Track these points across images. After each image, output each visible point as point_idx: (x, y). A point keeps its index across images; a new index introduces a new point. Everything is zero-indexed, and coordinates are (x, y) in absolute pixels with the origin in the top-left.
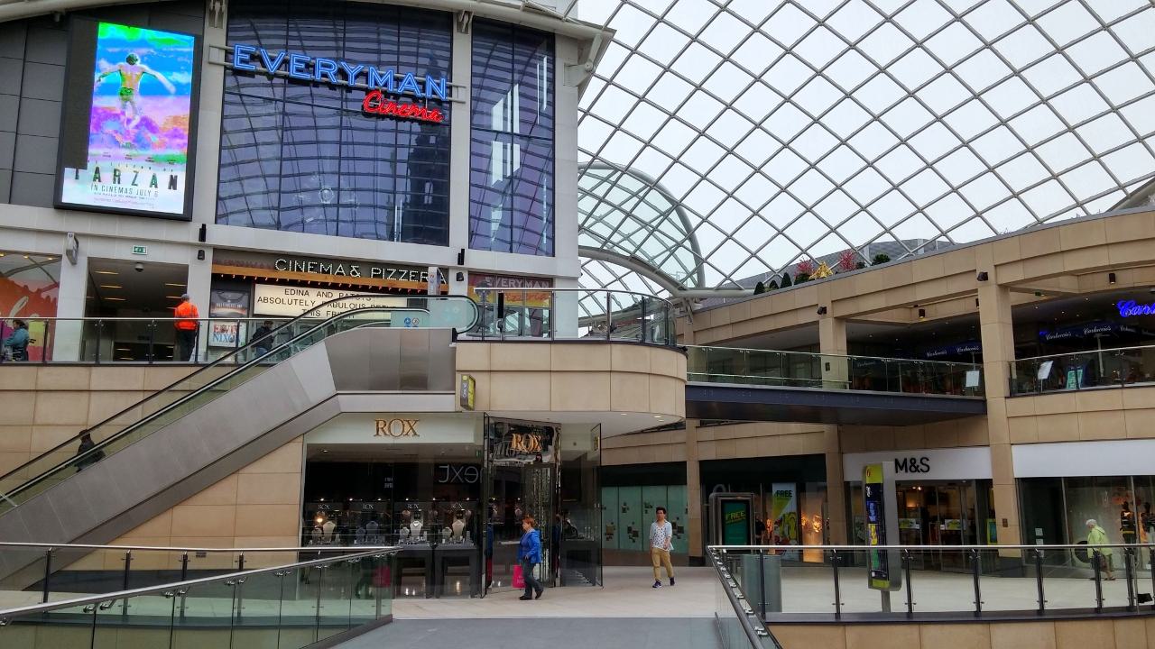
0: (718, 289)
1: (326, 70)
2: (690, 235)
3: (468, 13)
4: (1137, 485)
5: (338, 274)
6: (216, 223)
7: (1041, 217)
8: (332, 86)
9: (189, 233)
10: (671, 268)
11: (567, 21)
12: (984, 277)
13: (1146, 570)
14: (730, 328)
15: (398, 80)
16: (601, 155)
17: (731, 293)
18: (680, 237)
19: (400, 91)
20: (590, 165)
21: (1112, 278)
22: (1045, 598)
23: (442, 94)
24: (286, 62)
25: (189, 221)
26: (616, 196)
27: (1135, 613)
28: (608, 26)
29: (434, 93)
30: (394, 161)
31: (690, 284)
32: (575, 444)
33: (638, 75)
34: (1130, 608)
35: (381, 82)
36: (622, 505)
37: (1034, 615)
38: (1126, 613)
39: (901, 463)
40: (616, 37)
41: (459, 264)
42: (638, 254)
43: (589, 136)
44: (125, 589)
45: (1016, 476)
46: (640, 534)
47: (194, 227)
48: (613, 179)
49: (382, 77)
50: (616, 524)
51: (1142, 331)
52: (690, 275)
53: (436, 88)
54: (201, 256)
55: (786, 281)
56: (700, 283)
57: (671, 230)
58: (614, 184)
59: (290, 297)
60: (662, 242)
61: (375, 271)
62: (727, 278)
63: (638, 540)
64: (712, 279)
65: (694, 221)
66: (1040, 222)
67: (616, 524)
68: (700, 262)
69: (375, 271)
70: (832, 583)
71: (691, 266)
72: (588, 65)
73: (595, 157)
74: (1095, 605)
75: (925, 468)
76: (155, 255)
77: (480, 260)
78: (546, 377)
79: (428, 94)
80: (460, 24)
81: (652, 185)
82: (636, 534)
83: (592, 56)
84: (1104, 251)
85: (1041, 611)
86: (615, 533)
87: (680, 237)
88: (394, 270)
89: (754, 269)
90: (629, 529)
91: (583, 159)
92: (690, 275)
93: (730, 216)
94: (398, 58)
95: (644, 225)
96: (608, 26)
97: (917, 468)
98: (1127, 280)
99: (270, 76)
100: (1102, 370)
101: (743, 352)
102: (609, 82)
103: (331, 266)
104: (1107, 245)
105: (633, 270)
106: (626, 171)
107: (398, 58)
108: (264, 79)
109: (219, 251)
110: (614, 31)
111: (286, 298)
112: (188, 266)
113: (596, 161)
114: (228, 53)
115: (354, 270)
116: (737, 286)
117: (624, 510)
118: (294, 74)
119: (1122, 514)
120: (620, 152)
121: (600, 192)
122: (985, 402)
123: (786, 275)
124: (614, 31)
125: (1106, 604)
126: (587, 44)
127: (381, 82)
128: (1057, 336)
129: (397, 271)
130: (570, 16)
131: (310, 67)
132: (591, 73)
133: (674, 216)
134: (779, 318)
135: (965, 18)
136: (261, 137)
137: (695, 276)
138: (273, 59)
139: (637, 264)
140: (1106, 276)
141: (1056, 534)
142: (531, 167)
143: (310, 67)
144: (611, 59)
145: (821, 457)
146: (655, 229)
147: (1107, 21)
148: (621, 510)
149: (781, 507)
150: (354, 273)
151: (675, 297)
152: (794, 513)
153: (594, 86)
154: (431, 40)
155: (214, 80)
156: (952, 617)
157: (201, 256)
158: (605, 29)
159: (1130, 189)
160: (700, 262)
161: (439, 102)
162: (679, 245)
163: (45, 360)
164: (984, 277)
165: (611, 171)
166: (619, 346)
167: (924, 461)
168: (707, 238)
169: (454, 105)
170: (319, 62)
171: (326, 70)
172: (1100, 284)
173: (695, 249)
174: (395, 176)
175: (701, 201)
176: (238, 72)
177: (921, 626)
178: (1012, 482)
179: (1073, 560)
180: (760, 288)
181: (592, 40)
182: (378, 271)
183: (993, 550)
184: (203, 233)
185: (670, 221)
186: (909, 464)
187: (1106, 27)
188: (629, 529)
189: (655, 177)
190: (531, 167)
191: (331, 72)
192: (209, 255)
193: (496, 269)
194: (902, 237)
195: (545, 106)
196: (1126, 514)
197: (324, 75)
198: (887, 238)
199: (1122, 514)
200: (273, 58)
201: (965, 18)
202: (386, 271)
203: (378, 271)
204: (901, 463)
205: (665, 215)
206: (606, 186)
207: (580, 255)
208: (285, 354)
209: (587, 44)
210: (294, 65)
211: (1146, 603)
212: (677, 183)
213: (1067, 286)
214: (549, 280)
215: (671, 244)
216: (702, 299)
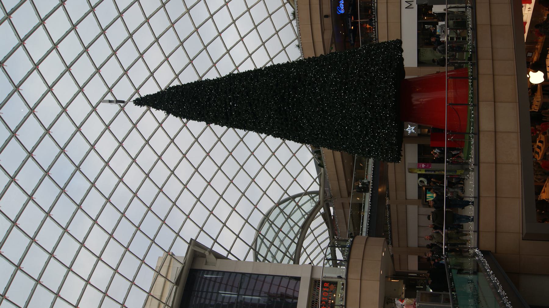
0: (320, 185)
2: (293, 198)
7: (295, 37)
10: (308, 207)
11: (185, 263)
17: (323, 179)
18: (293, 204)
21: (326, 16)
26: (270, 235)
31: (317, 199)
33: (213, 227)
40: (194, 238)
42: (300, 224)
43: (240, 251)
45: (416, 66)
51: (351, 3)
52: (312, 198)
56: (317, 193)
57: (290, 207)
58: (264, 237)
62: (315, 180)
64: (316, 187)
65: (286, 196)
66: (297, 38)
71: (307, 198)
72: (207, 253)
73: (251, 247)
81: (266, 217)
83: (202, 251)
84: (315, 26)
89: (312, 168)
91: (251, 258)
92: (312, 198)
93: (285, 179)
95: (287, 249)
98: (327, 10)
102: (215, 241)
104: (311, 24)
106: (259, 231)
110: (192, 239)
113: (254, 247)
116: (319, 177)
120: (249, 235)
121: (268, 244)
124: (192, 239)
126: (197, 252)
130: (182, 261)
132: (211, 251)
133: (282, 206)
137: (313, 195)
139: (305, 227)
142: (255, 285)
144: (206, 242)
153: (217, 249)
158: (190, 244)
160: (306, 193)
166: (349, 275)
168: (295, 190)
172: (328, 22)
173: (300, 195)
175: (276, 194)
181: (195, 251)
187: (135, 126)
189: (262, 216)
190: (255, 285)
195: (223, 295)
205: (282, 211)
207: (298, 264)
209: (197, 252)
212: (266, 206)
213: (329, 35)
216: (325, 192)
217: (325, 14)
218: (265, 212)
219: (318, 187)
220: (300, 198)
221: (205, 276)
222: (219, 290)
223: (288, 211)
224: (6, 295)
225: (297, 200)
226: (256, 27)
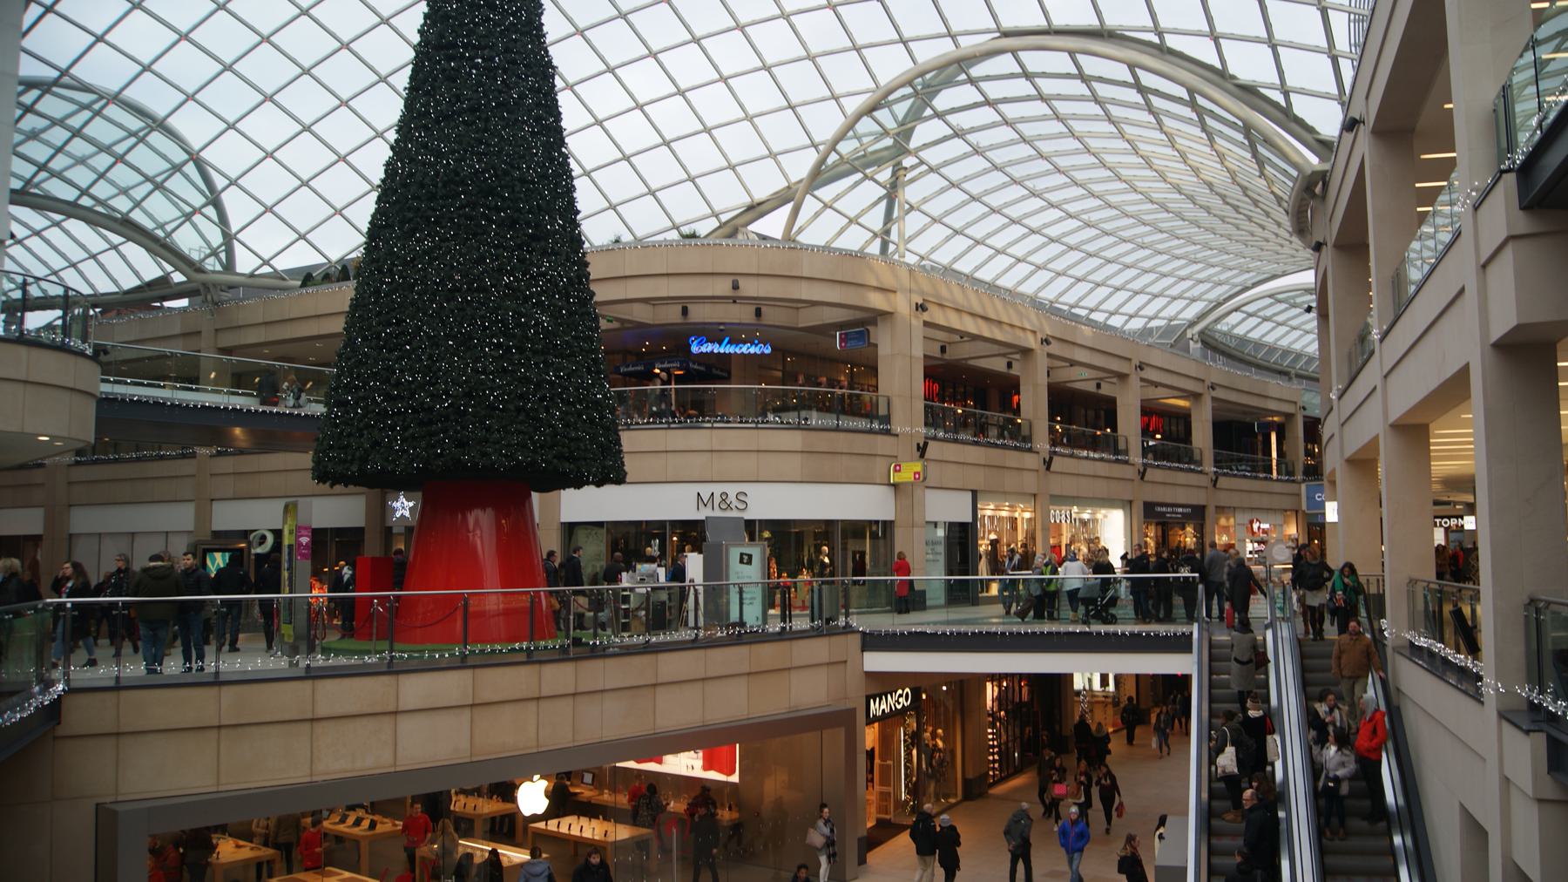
0: (252, 275)
4: (845, 537)
7: (639, 234)
14: (263, 329)
16: (72, 71)
17: (269, 285)
18: (198, 200)
20: (56, 82)
31: (212, 264)
44: (1187, 814)
45: (563, 520)
48: (97, 107)
55: (327, 278)
56: (229, 266)
58: (98, 113)
64: (245, 263)
65: (220, 182)
68: (228, 238)
71: (216, 238)
73: (64, 73)
75: (741, 506)
87: (198, 200)
89: (301, 257)
93: (269, 182)
105: (129, 239)
106: (116, 99)
113: (63, 81)
120: (103, 70)
121: (76, 122)
123: (345, 268)
133: (190, 169)
134: (632, 283)
140: (679, 308)
147: (307, 122)
151: (189, 280)
159: (724, 218)
160: (228, 238)
162: (196, 211)
165: (94, 97)
168: (237, 207)
172: (672, 315)
173: (223, 220)
175: (227, 156)
178: (556, 526)
185: (186, 177)
186: (717, 499)
194: (280, 268)
198: (266, 269)
205: (177, 168)
206: (87, 114)
207: (12, 202)
213: (642, 314)
215: (188, 209)
217: (742, 282)
218: (173, 122)
219: (247, 271)
220: (216, 219)
223: (176, 183)
225: (211, 211)
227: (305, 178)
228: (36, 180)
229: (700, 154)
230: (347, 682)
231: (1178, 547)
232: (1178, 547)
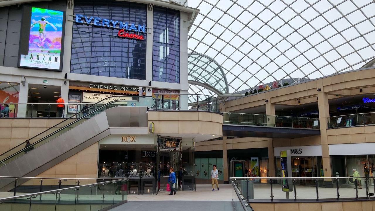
0: (233, 94)
1: (106, 23)
2: (224, 76)
3: (152, 4)
4: (369, 158)
5: (110, 89)
6: (70, 72)
7: (338, 70)
8: (108, 28)
9: (62, 76)
10: (218, 87)
11: (184, 7)
12: (320, 90)
13: (372, 185)
14: (237, 107)
15: (129, 26)
16: (195, 50)
17: (237, 95)
18: (221, 77)
19: (130, 30)
20: (191, 54)
21: (361, 90)
22: (339, 194)
23: (143, 31)
24: (93, 20)
25: (61, 72)
26: (200, 64)
27: (368, 199)
28: (198, 9)
29: (141, 30)
30: (128, 52)
31: (224, 92)
32: (187, 144)
33: (207, 24)
34: (367, 198)
35: (124, 27)
36: (202, 164)
37: (336, 200)
38: (366, 199)
39: (293, 150)
40: (200, 12)
41: (149, 86)
42: (207, 82)
43: (191, 44)
45: (330, 155)
46: (208, 174)
47: (63, 74)
48: (199, 58)
49: (124, 25)
50: (200, 170)
51: (371, 108)
52: (224, 89)
53: (142, 29)
54: (65, 83)
55: (255, 91)
56: (227, 92)
57: (218, 75)
58: (199, 60)
59: (94, 97)
60: (215, 79)
61: (122, 88)
62: (236, 90)
63: (207, 176)
64: (231, 91)
65: (225, 72)
66: (338, 72)
67: (200, 170)
68: (227, 85)
69: (122, 88)
70: (270, 190)
71: (224, 86)
72: (191, 21)
73: (193, 51)
74: (356, 197)
75: (300, 152)
76: (50, 83)
77: (156, 84)
78: (177, 122)
79: (139, 31)
80: (149, 8)
81: (212, 60)
82: (206, 174)
83: (192, 18)
84: (358, 82)
85: (338, 199)
86: (200, 173)
87: (221, 77)
88: (128, 88)
89: (245, 88)
90: (204, 172)
92: (224, 89)
93: (237, 70)
94: (129, 19)
96: (198, 9)
97: (298, 152)
98: (366, 91)
99: (88, 25)
100: (358, 120)
101: (241, 114)
102: (198, 27)
103: (107, 87)
104: (359, 80)
105: (205, 88)
106: (203, 55)
107: (129, 19)
108: (86, 26)
109: (71, 82)
110: (199, 10)
111: (93, 97)
112: (61, 86)
113: (193, 52)
114: (74, 17)
115: (115, 88)
116: (239, 93)
117: (203, 166)
118: (95, 24)
119: (364, 167)
120: (201, 49)
121: (195, 62)
122: (320, 131)
123: (255, 89)
124: (199, 10)
125: (359, 196)
126: (191, 14)
127: (124, 27)
128: (343, 109)
129: (129, 88)
130: (185, 5)
131: (101, 22)
132: (192, 24)
133: (219, 70)
134: (253, 103)
135: (313, 6)
136: (85, 44)
137: (226, 90)
138: (88, 19)
139: (207, 86)
140: (359, 90)
141: (343, 174)
142: (172, 54)
143: (101, 22)
144: (198, 19)
145: (267, 149)
146: (213, 74)
148: (202, 166)
149: (253, 165)
150: (115, 89)
151: (219, 96)
152: (258, 167)
153: (193, 28)
154: (140, 13)
155: (70, 26)
156: (309, 201)
157: (65, 83)
158: (197, 9)
159: (367, 62)
160: (227, 85)
161: (143, 33)
162: (220, 80)
163: (15, 117)
164: (320, 90)
165: (198, 56)
167: (300, 150)
168: (229, 78)
169: (147, 34)
170: (104, 20)
171: (106, 23)
172: (357, 92)
173: (226, 81)
174: (128, 57)
175: (228, 65)
176: (77, 24)
177: (299, 204)
178: (329, 157)
179: (348, 182)
180: (247, 94)
181: (192, 13)
182: (123, 88)
183: (322, 179)
184: (66, 76)
185: (218, 72)
186: (295, 151)
188: (204, 172)
189: (213, 57)
190: (172, 54)
191: (107, 24)
192: (68, 83)
193: (161, 87)
194: (293, 77)
196: (366, 167)
197: (105, 24)
198: (288, 77)
199: (364, 167)
200: (89, 19)
201: (313, 6)
202: (125, 88)
203: (123, 88)
204: (293, 150)
205: (216, 70)
206: (197, 60)
208: (93, 115)
209: (191, 14)
210: (95, 21)
211: (372, 196)
212: (220, 59)
213: (347, 93)
214: (178, 91)
215: (218, 79)
216: (228, 97)
221: (177, 19)
222: (169, 27)
224: (129, 56)
226: (322, 55)
227: (302, 52)
228: (190, 73)
229: (345, 50)
230: (308, 204)
231: (126, 190)
232: (126, 190)
